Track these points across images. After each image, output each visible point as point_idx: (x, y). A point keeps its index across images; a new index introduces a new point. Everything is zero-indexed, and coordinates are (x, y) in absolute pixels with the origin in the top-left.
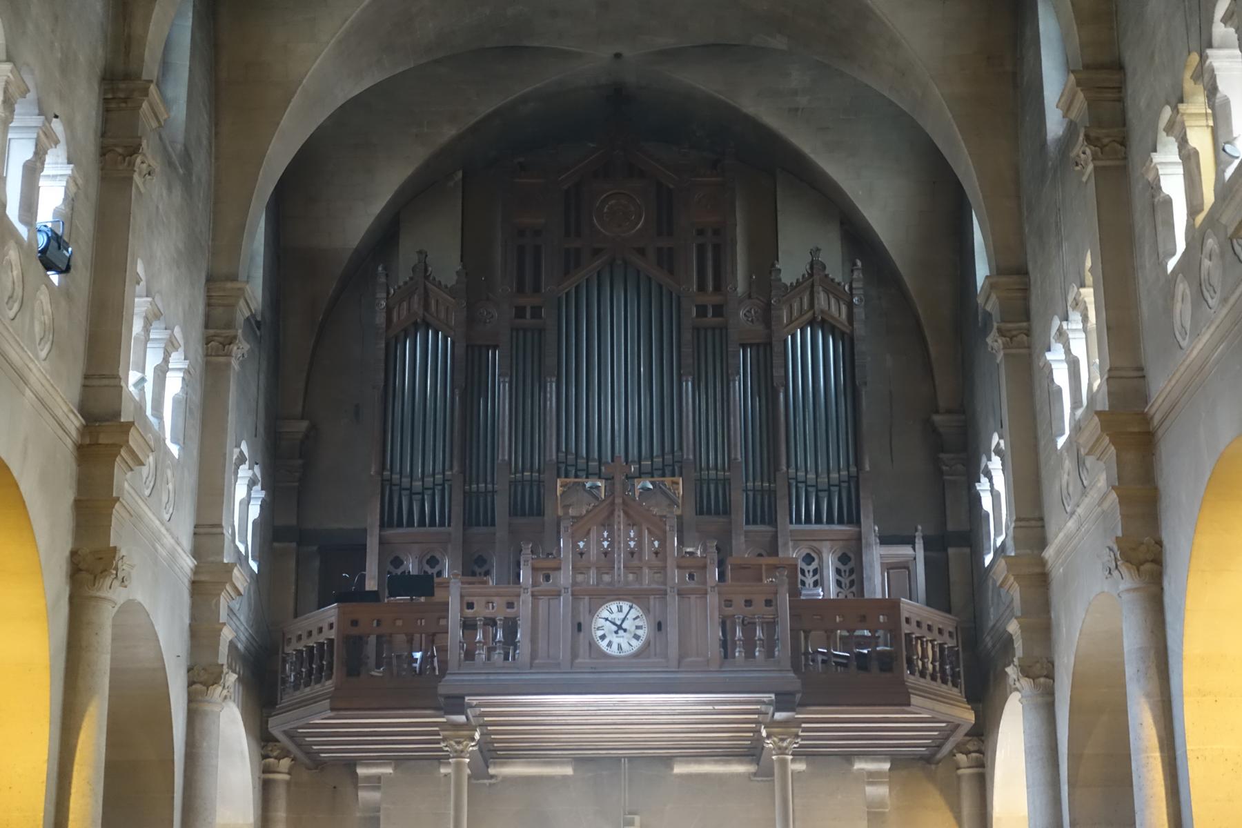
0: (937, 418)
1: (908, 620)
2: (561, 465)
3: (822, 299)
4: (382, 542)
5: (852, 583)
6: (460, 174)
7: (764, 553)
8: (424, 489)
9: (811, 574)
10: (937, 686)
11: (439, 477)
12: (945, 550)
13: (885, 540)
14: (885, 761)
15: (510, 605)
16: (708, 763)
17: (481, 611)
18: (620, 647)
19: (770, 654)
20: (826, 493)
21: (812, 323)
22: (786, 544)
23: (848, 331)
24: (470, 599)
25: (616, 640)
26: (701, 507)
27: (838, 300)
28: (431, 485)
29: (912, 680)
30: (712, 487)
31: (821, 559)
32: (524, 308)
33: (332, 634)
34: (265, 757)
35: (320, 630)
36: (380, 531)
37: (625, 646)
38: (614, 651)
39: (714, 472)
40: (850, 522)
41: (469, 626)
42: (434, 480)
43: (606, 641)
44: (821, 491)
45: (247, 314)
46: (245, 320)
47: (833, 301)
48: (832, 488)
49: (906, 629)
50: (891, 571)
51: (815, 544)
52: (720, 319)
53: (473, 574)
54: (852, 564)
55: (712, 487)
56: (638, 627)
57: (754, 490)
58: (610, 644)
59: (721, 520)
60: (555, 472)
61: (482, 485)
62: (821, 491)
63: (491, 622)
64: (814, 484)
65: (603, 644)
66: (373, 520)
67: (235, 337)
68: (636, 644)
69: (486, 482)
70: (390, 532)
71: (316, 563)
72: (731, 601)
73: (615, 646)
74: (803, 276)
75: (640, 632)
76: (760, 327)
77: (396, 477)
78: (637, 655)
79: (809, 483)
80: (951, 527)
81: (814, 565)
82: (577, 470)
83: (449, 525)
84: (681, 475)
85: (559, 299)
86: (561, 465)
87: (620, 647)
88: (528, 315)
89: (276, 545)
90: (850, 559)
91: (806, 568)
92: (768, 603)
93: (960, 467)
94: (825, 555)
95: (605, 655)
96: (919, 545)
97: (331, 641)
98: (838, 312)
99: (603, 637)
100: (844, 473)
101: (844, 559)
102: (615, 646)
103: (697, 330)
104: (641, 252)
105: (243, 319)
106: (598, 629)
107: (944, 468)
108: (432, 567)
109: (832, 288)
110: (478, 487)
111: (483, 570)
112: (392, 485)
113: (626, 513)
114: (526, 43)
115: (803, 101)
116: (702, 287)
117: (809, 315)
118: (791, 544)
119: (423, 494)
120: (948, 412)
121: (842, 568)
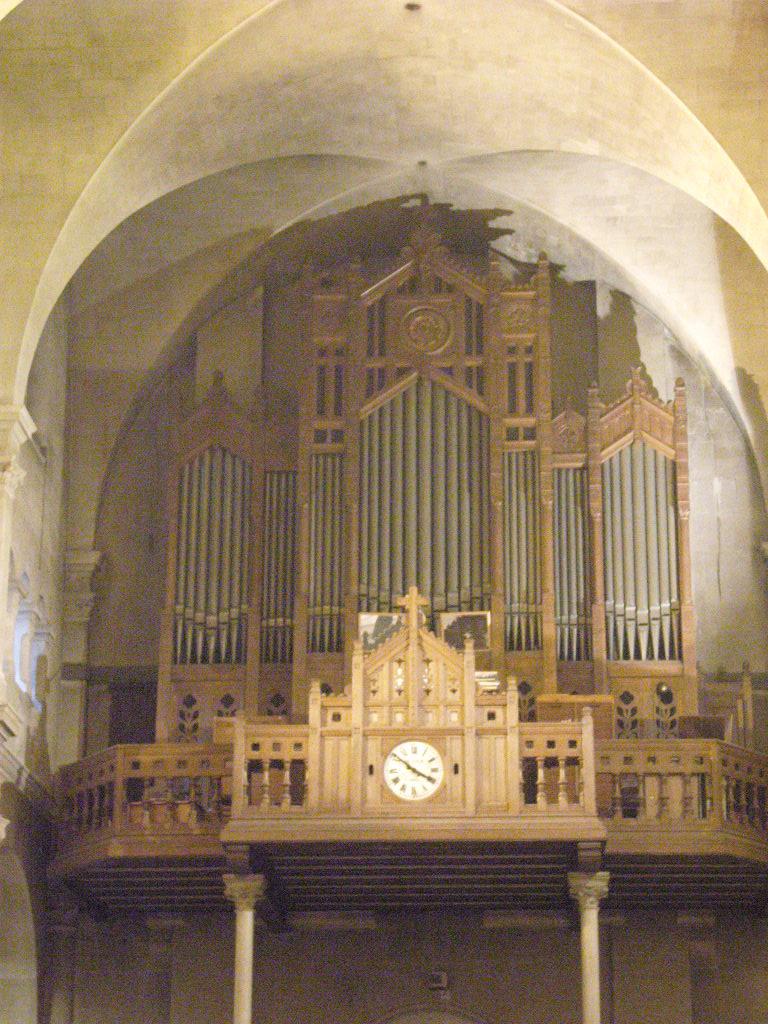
2: (362, 598)
6: (260, 291)
8: (230, 619)
9: (629, 713)
15: (298, 746)
17: (267, 754)
18: (414, 792)
19: (574, 799)
20: (647, 627)
24: (257, 740)
26: (512, 642)
28: (226, 620)
32: (325, 432)
37: (419, 790)
38: (407, 796)
39: (525, 605)
41: (254, 767)
42: (649, 612)
43: (399, 785)
44: (641, 625)
45: (23, 439)
46: (22, 446)
48: (653, 622)
52: (339, 446)
53: (270, 713)
56: (434, 770)
57: (569, 624)
58: (403, 788)
59: (336, 655)
60: (356, 607)
61: (280, 620)
62: (641, 625)
63: (277, 764)
64: (633, 617)
65: (396, 789)
67: (9, 464)
68: (432, 789)
69: (332, 604)
71: (107, 703)
72: (532, 742)
73: (408, 792)
75: (434, 775)
77: (620, 606)
78: (431, 800)
79: (628, 616)
82: (379, 603)
84: (490, 609)
86: (362, 598)
87: (414, 792)
88: (329, 440)
89: (63, 682)
91: (624, 707)
92: (573, 744)
95: (399, 800)
99: (396, 781)
100: (574, 617)
104: (449, 371)
105: (18, 445)
106: (391, 771)
108: (627, 703)
110: (276, 622)
111: (229, 710)
112: (615, 616)
114: (325, 150)
115: (621, 209)
119: (660, 619)
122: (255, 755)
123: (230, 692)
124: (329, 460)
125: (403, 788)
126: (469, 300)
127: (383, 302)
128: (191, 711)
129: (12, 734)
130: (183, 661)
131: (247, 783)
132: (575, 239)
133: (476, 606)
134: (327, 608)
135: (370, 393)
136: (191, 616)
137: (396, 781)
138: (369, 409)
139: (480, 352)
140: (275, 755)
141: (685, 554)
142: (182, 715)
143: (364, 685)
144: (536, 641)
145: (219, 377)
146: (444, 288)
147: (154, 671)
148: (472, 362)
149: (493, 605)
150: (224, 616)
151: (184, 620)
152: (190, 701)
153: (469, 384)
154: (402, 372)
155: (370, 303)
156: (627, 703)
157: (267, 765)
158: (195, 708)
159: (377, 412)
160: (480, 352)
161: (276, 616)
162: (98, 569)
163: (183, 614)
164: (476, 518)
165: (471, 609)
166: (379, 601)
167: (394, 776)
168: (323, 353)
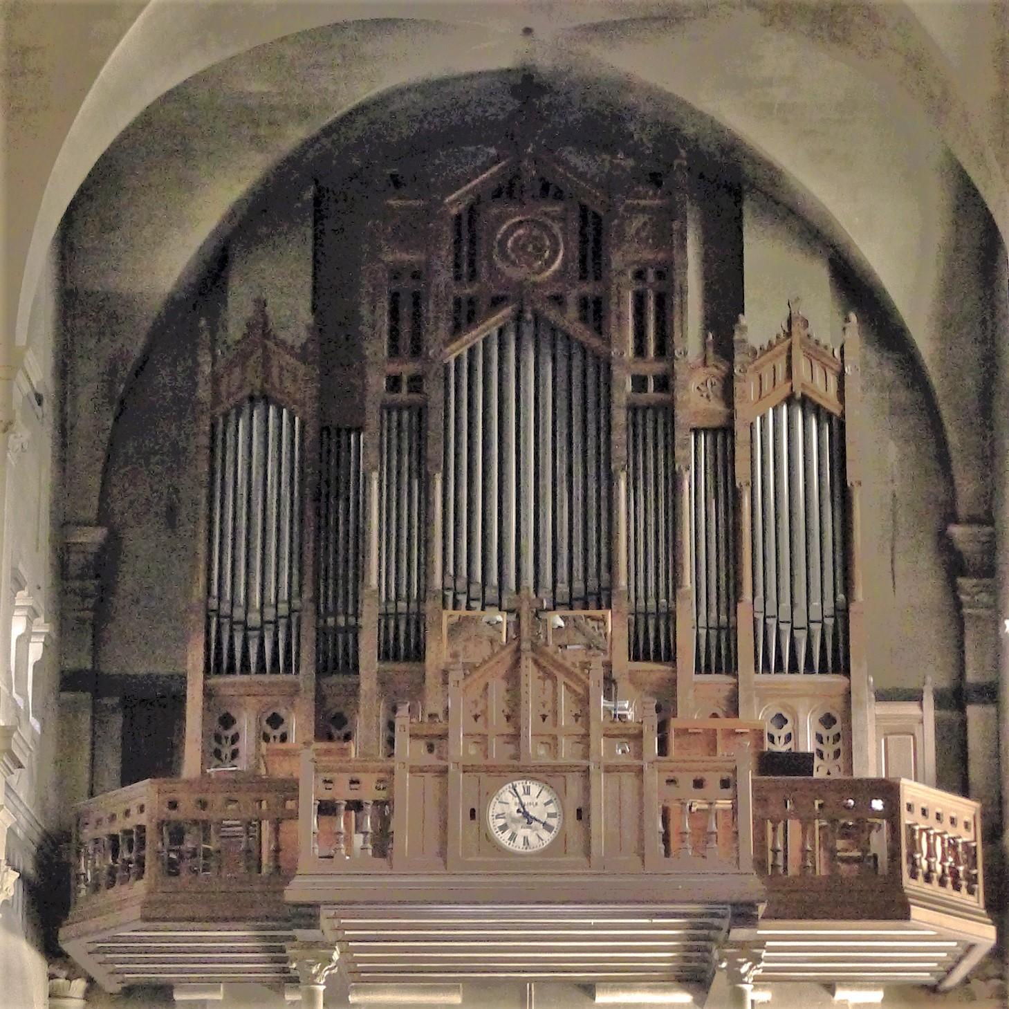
0: (956, 531)
1: (910, 807)
3: (801, 365)
4: (208, 694)
5: (837, 754)
7: (720, 713)
8: (277, 617)
9: (783, 740)
10: (948, 893)
11: (283, 609)
12: (962, 709)
13: (883, 696)
14: (876, 988)
16: (642, 989)
21: (789, 400)
22: (749, 701)
23: (837, 412)
25: (522, 832)
27: (824, 367)
29: (910, 885)
30: (651, 622)
31: (796, 721)
33: (143, 819)
34: (52, 977)
35: (127, 813)
36: (205, 678)
37: (533, 839)
38: (518, 846)
40: (836, 670)
47: (818, 371)
49: (906, 819)
50: (889, 737)
51: (785, 700)
54: (837, 728)
55: (651, 622)
56: (550, 815)
58: (513, 837)
66: (195, 658)
68: (547, 837)
70: (215, 680)
73: (520, 840)
74: (778, 337)
76: (718, 407)
77: (225, 608)
78: (546, 852)
80: (971, 676)
81: (787, 729)
83: (297, 670)
85: (447, 367)
88: (405, 388)
90: (834, 721)
93: (984, 597)
94: (801, 717)
96: (929, 700)
97: (141, 829)
98: (824, 390)
99: (504, 828)
101: (828, 721)
102: (520, 840)
103: (633, 409)
104: (558, 300)
106: (498, 817)
107: (963, 597)
109: (815, 351)
110: (336, 621)
113: (536, 662)
116: (640, 351)
117: (784, 391)
118: (756, 700)
120: (972, 520)
121: (824, 733)
122: (327, 796)
123: (277, 710)
124: (395, 415)
125: (513, 837)
126: (584, 209)
127: (472, 210)
128: (230, 733)
129: (21, 766)
130: (218, 671)
131: (663, 830)
132: (718, 129)
133: (592, 604)
134: (402, 605)
135: (457, 330)
136: (215, 607)
137: (504, 828)
138: (459, 349)
139: (598, 278)
140: (353, 796)
141: (615, 506)
142: (218, 738)
143: (966, 730)
144: (668, 648)
145: (261, 304)
146: (551, 192)
147: (183, 679)
148: (588, 288)
149: (614, 601)
150: (270, 614)
151: (232, 623)
152: (227, 721)
153: (583, 319)
154: (497, 302)
155: (454, 211)
156: (227, 727)
157: (343, 807)
158: (282, 729)
159: (466, 354)
160: (598, 278)
161: (335, 614)
162: (103, 548)
163: (231, 617)
164: (838, 526)
165: (586, 607)
166: (468, 596)
167: (501, 822)
168: (396, 275)
